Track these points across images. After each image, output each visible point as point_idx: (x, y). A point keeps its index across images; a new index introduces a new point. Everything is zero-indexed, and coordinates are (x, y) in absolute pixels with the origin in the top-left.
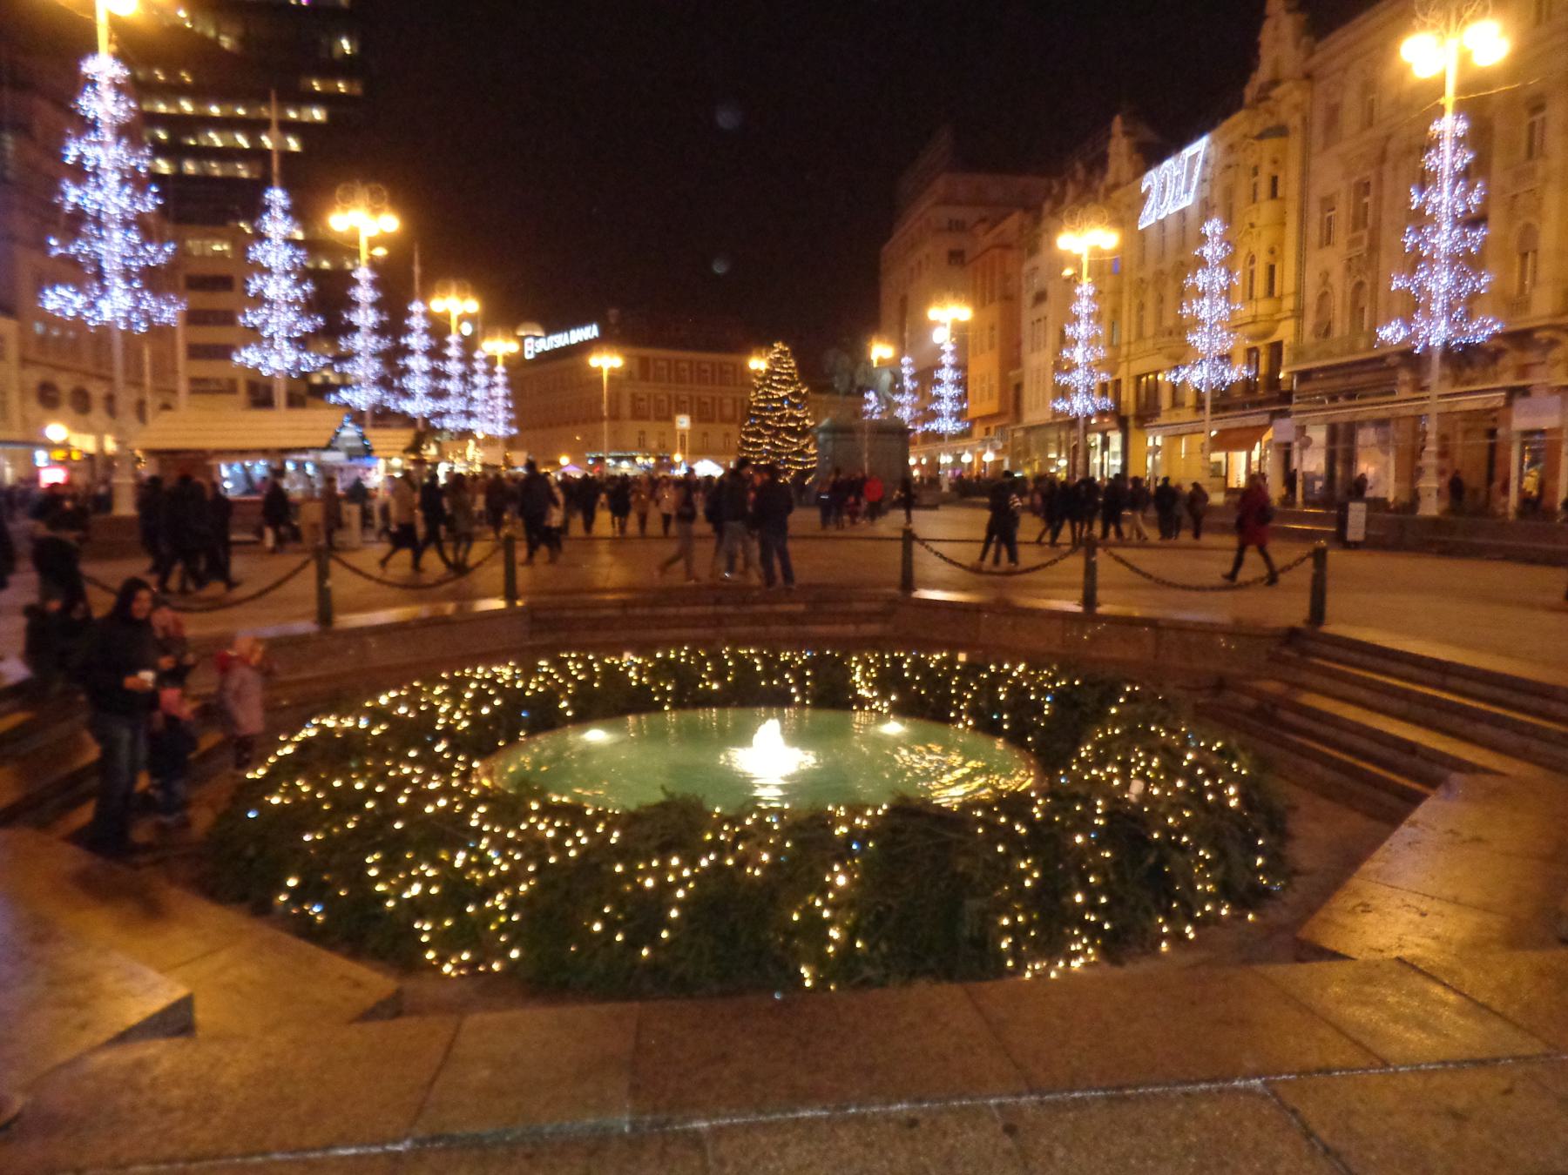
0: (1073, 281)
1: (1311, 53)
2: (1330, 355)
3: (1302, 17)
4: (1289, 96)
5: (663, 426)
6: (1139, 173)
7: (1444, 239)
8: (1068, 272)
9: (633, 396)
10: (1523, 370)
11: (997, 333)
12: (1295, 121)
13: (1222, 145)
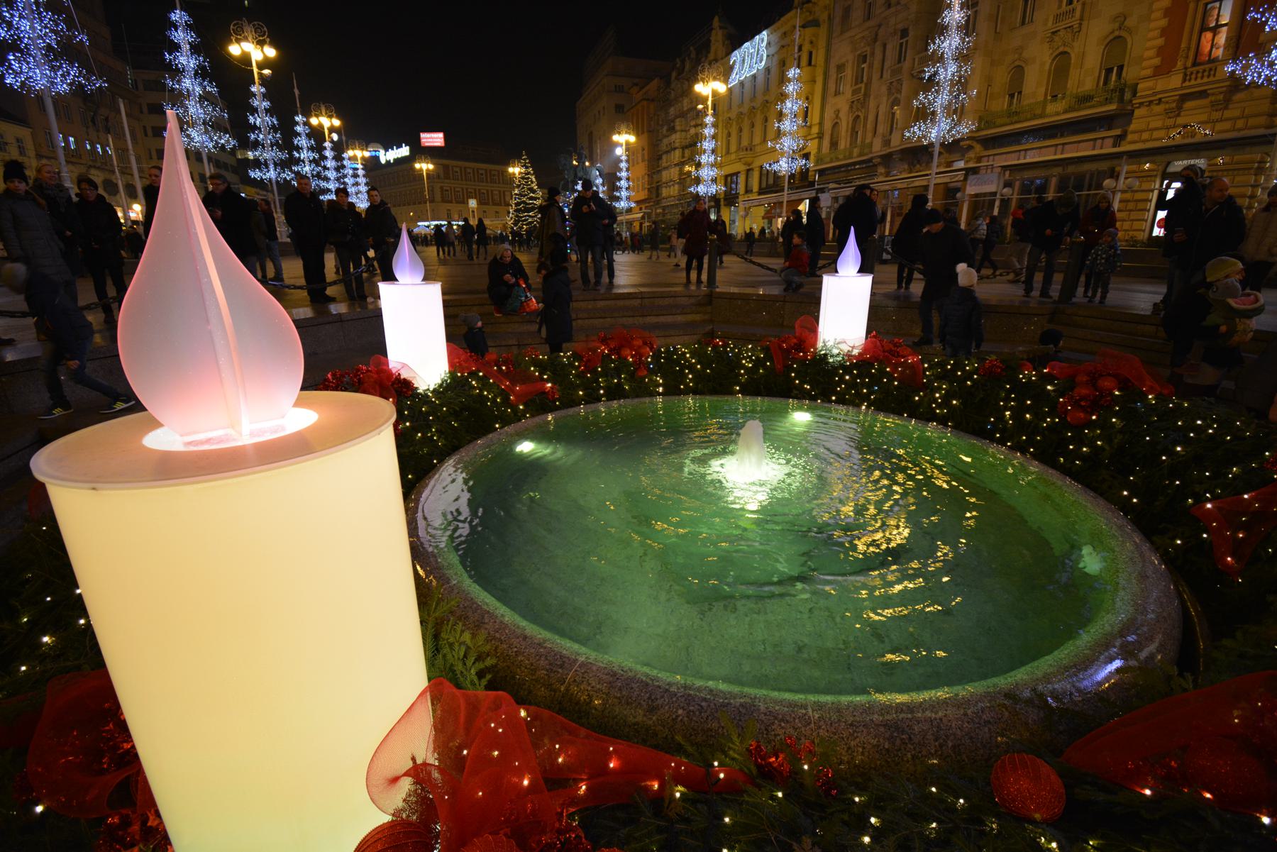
0: (704, 113)
2: (838, 159)
5: (460, 207)
6: (729, 53)
7: (948, 71)
8: (700, 107)
9: (442, 188)
10: (979, 159)
11: (646, 152)
12: (823, 17)
13: (779, 34)
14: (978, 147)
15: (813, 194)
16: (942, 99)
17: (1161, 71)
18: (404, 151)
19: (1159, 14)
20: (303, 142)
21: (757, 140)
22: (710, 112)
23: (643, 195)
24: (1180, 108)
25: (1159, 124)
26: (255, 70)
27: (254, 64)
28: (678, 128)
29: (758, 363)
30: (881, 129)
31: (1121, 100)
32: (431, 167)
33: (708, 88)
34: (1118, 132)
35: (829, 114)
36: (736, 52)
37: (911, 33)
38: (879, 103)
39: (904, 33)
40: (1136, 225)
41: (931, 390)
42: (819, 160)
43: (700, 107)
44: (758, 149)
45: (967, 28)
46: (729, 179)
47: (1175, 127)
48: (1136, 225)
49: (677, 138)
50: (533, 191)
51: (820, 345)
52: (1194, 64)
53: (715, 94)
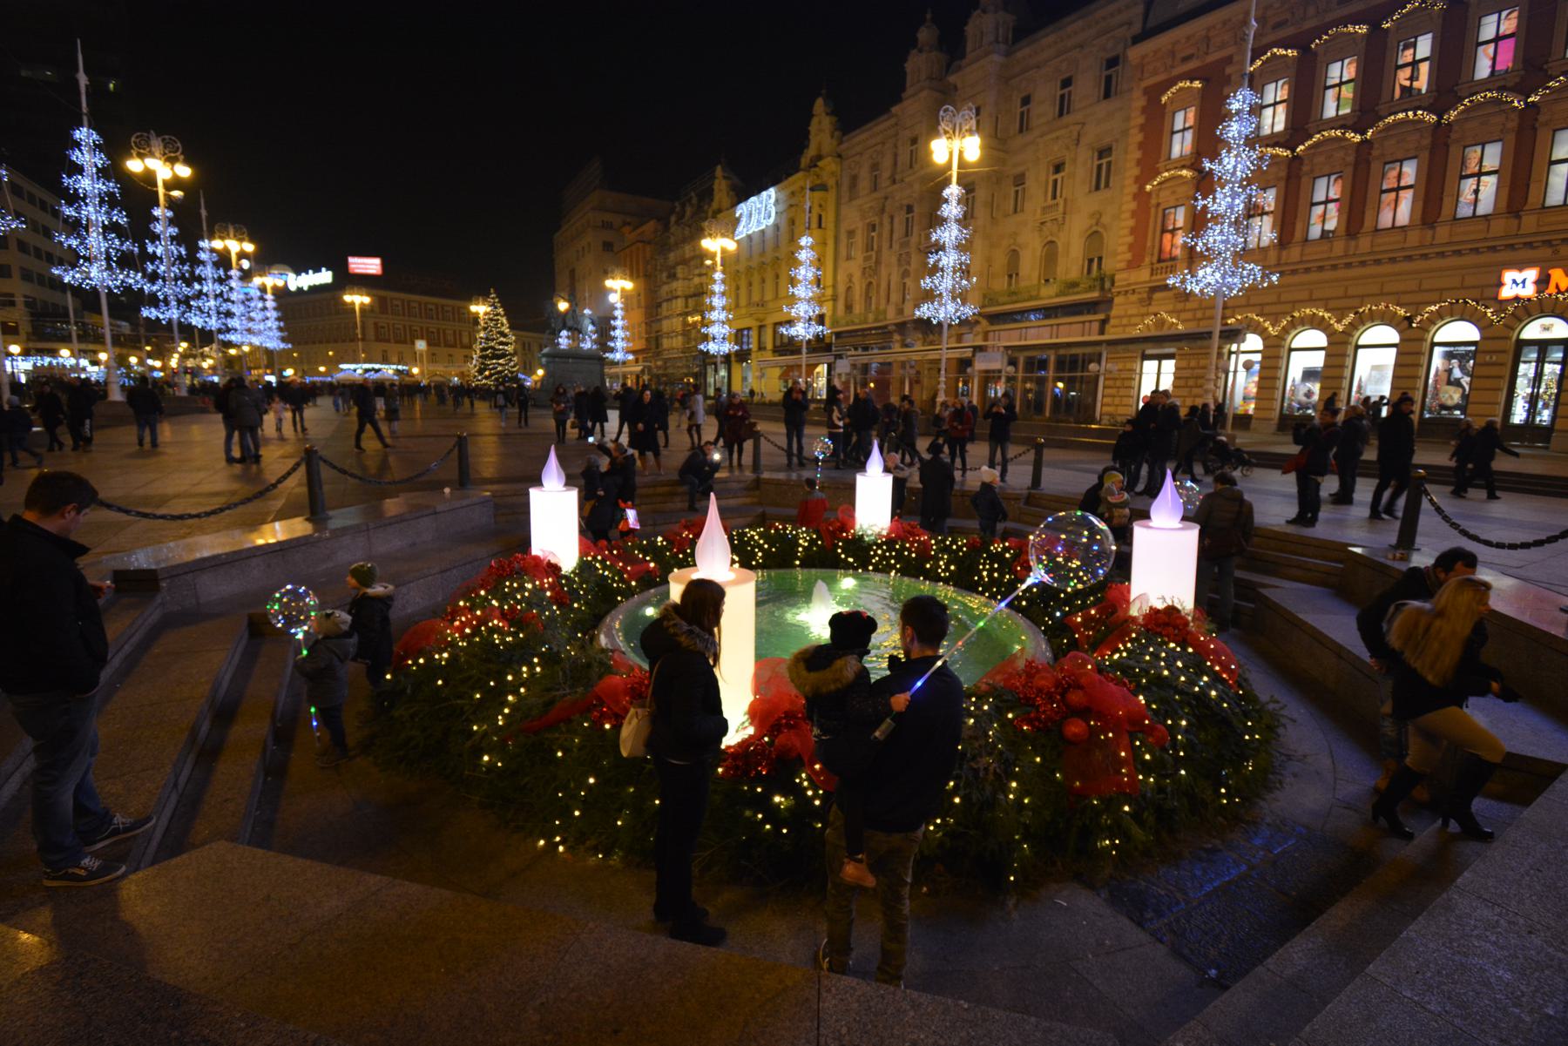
0: (713, 268)
1: (840, 143)
2: (853, 323)
3: (834, 119)
4: (829, 165)
7: (949, 259)
8: (708, 262)
9: (376, 324)
12: (831, 182)
13: (788, 192)
14: (984, 322)
15: (831, 359)
16: (946, 283)
17: (1133, 264)
18: (325, 277)
19: (1127, 215)
20: (208, 271)
21: (769, 296)
22: (719, 268)
23: (640, 345)
24: (1150, 298)
25: (1134, 311)
26: (161, 191)
27: (160, 184)
28: (680, 275)
29: (812, 542)
30: (894, 297)
31: (1102, 288)
32: (367, 300)
33: (715, 245)
34: (1102, 316)
35: (841, 277)
36: (742, 205)
37: (916, 209)
38: (890, 272)
39: (910, 209)
40: (1125, 401)
41: (936, 559)
42: (835, 323)
43: (708, 262)
44: (771, 305)
45: (963, 222)
46: (738, 336)
47: (1148, 314)
48: (1125, 401)
49: (678, 286)
50: (505, 335)
51: (857, 527)
52: (1159, 261)
53: (724, 251)
